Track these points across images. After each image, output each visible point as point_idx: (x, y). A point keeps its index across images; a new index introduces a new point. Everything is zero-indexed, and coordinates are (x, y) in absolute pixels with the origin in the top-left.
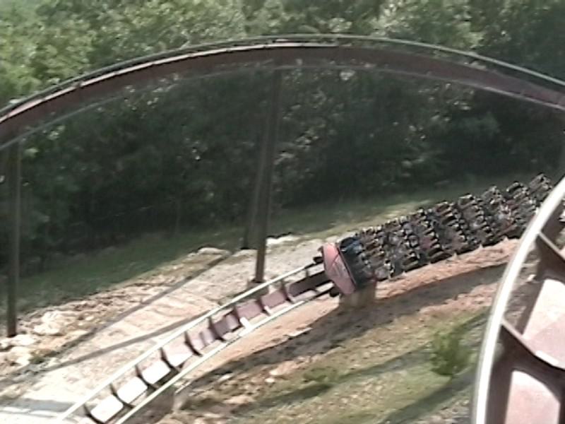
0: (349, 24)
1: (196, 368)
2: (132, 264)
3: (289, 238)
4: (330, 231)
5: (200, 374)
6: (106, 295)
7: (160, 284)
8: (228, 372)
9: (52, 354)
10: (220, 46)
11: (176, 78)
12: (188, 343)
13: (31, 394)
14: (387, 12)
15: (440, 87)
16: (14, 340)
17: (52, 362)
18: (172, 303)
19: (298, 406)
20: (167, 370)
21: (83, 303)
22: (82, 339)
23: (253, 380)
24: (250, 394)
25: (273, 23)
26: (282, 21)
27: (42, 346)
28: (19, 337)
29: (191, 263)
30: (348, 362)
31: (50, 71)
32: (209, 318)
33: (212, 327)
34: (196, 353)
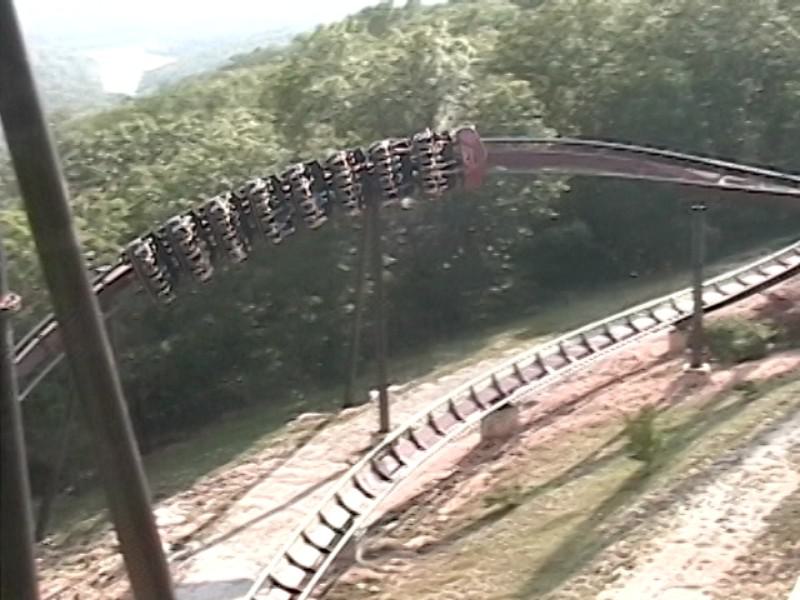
1: (369, 513)
8: (394, 519)
17: (194, 545)
20: (347, 516)
23: (425, 521)
29: (293, 432)
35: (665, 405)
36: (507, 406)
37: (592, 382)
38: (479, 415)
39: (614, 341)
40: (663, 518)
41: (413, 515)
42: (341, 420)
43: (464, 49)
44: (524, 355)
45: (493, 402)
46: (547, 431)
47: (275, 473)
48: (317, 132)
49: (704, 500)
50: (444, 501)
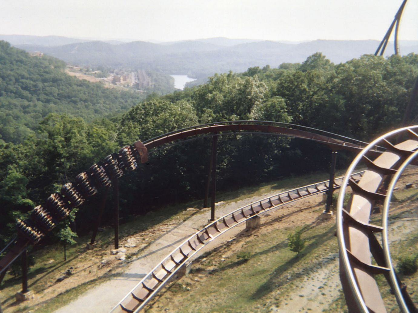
0: (239, 117)
1: (193, 255)
2: (160, 217)
3: (222, 202)
4: (238, 198)
5: (194, 259)
6: (152, 230)
7: (174, 224)
9: (134, 254)
10: (189, 129)
11: (173, 142)
12: (190, 245)
13: (127, 272)
14: (253, 111)
15: (277, 139)
16: (118, 250)
17: (134, 257)
18: (180, 231)
19: (236, 269)
20: (182, 257)
21: (143, 233)
22: (145, 248)
24: (215, 266)
25: (210, 119)
26: (213, 117)
27: (130, 252)
28: (120, 249)
29: (184, 215)
30: (253, 250)
31: (124, 143)
32: (197, 235)
33: (198, 238)
34: (193, 249)
35: (314, 225)
36: (256, 217)
37: (291, 210)
38: (245, 219)
39: (300, 196)
40: (297, 282)
41: (212, 256)
42: (201, 213)
43: (263, 86)
44: (274, 195)
45: (251, 215)
46: (270, 228)
47: (172, 231)
48: (206, 111)
49: (316, 276)
50: (226, 252)
